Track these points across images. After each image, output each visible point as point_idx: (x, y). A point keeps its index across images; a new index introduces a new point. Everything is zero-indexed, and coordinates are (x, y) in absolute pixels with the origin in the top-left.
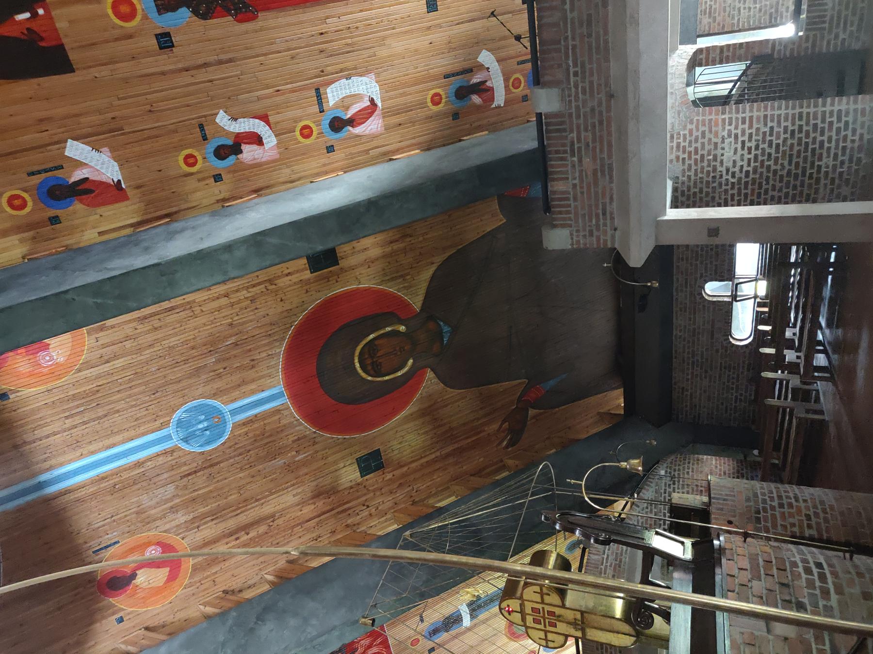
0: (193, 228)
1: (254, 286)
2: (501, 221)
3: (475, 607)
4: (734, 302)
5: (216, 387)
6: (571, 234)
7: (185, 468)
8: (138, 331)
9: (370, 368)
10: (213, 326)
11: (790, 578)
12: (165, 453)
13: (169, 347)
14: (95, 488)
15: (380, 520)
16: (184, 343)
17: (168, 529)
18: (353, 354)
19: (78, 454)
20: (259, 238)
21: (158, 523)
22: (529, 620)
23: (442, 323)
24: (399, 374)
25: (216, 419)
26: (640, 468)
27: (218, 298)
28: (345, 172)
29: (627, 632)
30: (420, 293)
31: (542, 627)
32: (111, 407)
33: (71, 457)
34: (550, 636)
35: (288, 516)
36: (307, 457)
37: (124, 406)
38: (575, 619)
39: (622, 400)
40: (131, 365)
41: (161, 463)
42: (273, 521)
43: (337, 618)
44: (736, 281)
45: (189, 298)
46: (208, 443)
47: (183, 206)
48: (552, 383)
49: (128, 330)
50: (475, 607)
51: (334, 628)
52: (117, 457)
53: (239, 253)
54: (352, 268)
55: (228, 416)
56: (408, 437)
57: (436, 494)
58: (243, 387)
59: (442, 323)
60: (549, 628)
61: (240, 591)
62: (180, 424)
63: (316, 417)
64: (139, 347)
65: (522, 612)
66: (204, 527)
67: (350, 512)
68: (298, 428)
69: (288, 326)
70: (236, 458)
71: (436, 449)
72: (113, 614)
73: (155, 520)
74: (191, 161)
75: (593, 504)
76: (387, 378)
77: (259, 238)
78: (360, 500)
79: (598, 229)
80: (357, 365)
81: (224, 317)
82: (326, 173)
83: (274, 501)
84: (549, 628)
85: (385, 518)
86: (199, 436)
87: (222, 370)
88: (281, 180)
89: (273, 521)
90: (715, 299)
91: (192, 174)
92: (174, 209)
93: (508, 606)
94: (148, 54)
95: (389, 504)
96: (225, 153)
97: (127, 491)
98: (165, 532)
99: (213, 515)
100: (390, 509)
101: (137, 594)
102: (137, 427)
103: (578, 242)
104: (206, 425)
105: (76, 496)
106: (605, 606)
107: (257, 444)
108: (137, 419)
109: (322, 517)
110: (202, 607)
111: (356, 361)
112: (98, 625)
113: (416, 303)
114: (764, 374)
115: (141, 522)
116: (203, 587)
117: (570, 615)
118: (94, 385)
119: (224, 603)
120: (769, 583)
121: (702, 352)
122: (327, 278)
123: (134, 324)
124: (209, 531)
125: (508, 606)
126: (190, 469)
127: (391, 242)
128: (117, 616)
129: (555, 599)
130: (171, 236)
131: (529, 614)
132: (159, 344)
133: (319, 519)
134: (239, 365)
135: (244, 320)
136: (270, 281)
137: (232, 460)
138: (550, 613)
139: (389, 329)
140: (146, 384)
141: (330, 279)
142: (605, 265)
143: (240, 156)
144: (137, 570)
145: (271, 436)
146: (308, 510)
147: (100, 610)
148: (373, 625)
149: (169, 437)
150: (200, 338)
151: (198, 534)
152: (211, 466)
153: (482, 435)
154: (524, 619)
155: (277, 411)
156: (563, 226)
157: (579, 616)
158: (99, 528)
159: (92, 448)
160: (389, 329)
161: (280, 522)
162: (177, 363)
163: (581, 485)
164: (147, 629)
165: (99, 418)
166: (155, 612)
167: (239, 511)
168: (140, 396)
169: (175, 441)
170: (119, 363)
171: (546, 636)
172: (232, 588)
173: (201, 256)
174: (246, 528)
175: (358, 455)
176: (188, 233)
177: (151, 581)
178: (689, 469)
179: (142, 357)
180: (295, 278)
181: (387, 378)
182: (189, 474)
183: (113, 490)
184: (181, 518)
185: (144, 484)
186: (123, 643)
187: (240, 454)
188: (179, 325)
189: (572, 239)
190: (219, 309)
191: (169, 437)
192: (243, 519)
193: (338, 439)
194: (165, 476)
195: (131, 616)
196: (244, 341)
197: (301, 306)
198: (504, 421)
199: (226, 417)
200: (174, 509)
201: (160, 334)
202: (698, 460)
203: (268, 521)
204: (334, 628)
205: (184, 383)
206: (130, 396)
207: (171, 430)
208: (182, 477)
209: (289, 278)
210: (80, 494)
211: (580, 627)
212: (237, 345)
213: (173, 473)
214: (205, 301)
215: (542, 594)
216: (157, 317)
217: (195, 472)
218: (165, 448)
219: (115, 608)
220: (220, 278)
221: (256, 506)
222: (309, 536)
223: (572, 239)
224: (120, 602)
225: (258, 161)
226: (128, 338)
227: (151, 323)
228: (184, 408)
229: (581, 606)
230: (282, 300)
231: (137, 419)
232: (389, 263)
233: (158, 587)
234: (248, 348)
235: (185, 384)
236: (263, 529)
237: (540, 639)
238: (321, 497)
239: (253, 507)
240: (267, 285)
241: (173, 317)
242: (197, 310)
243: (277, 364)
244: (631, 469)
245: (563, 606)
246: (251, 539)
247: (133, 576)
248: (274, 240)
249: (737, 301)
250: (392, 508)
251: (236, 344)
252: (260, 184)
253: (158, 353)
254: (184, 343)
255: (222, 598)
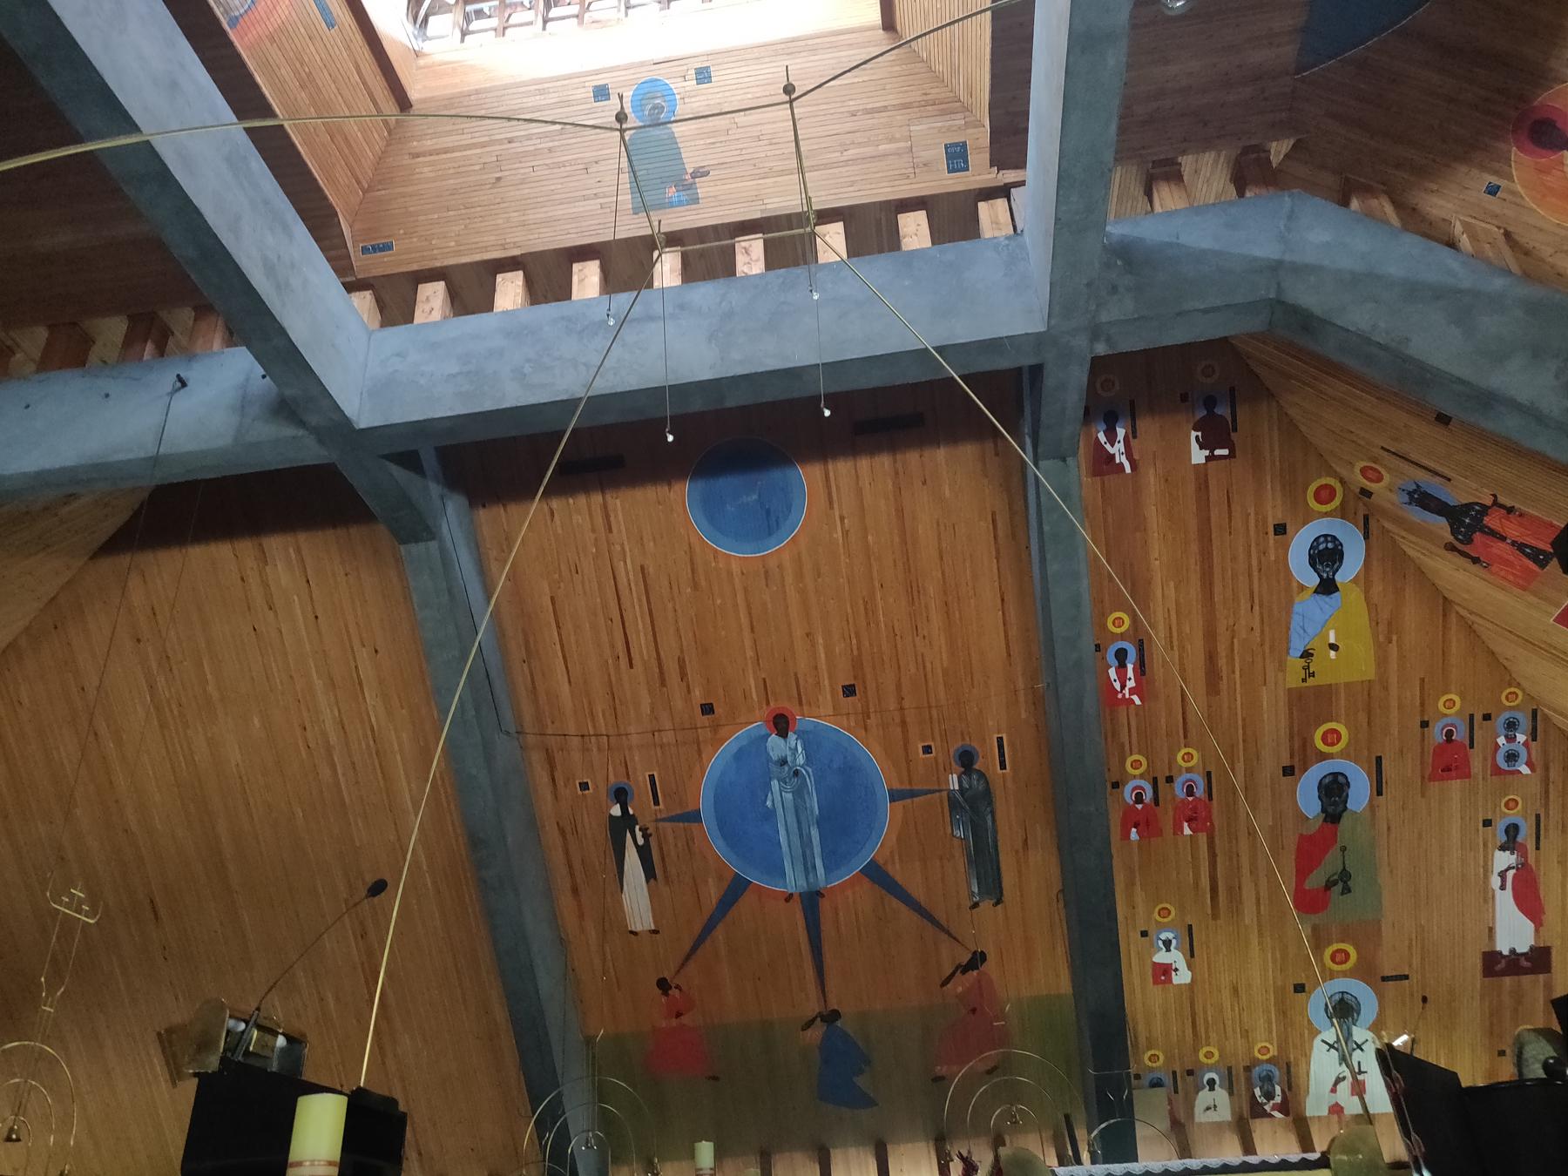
72: (1496, 173)
94: (780, 94)
128: (1495, 180)
164: (1507, 235)
195: (1509, 197)
219: (1506, 168)
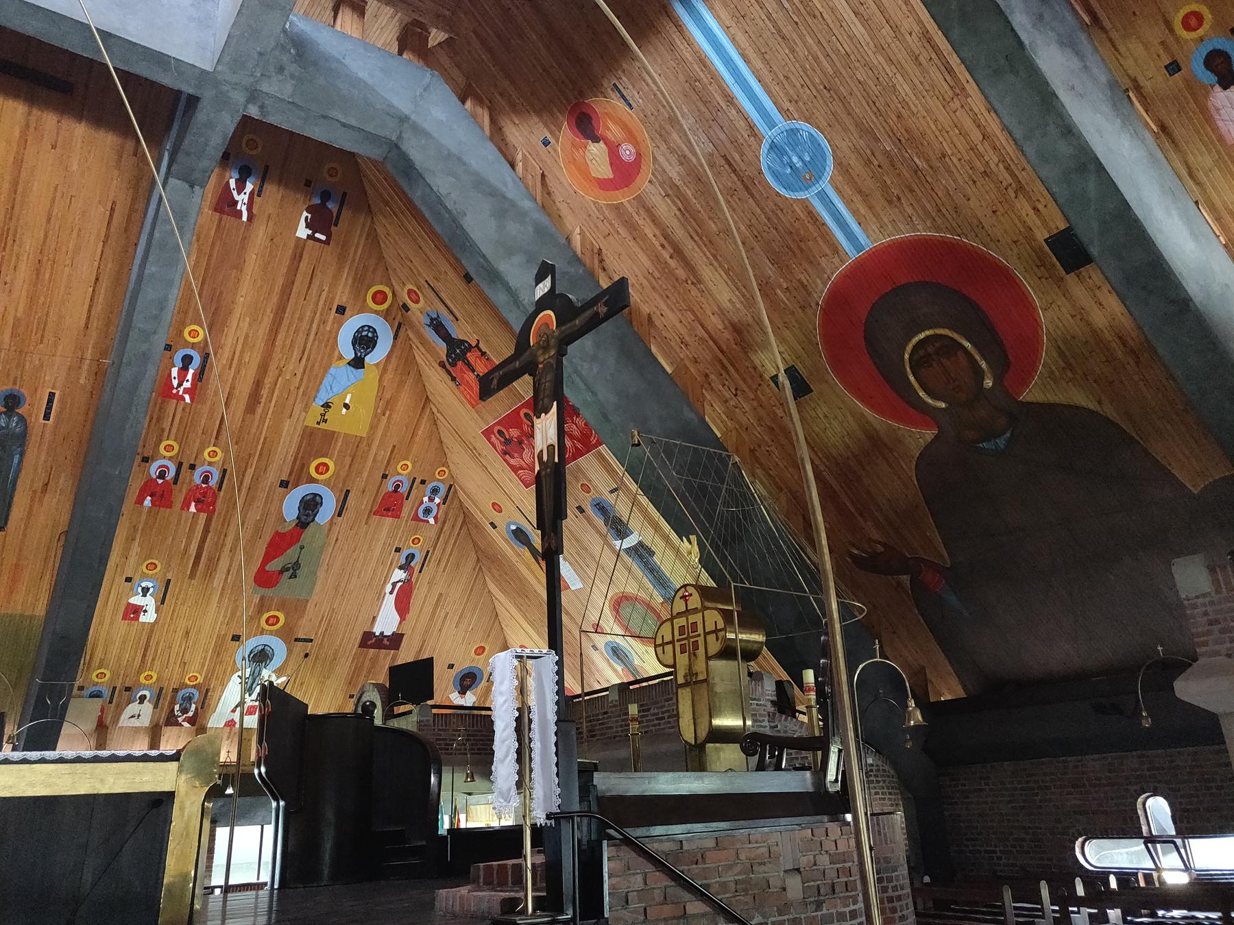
0: (1086, 67)
1: (1007, 168)
2: (1194, 486)
3: (641, 552)
4: (1143, 840)
5: (851, 162)
6: (1204, 595)
7: (737, 157)
8: (908, 37)
9: (921, 353)
10: (937, 133)
11: (841, 895)
12: (751, 127)
13: (894, 86)
14: (690, 59)
15: (722, 414)
16: (903, 104)
17: (657, 160)
18: (936, 327)
19: (728, 23)
20: (1092, 167)
21: (663, 147)
22: (681, 621)
23: (1008, 435)
24: (922, 394)
25: (811, 174)
26: (912, 722)
27: (979, 126)
28: (1225, 246)
29: (699, 735)
30: (1048, 396)
31: (677, 637)
32: (798, 41)
33: (723, 17)
34: (669, 648)
35: (702, 299)
36: (784, 302)
37: (801, 54)
38: (697, 674)
39: (949, 698)
40: (858, 46)
41: (738, 126)
42: (693, 283)
43: (607, 395)
44: (1179, 841)
45: (972, 88)
46: (775, 175)
47: (1114, 35)
48: (953, 599)
49: (907, 24)
50: (641, 552)
51: (594, 394)
52: (728, 62)
53: (1064, 148)
54: (1066, 294)
55: (815, 190)
56: (835, 424)
57: (770, 476)
58: (859, 198)
59: (1008, 435)
60: (677, 645)
61: (604, 269)
62: (793, 132)
63: (839, 299)
64: (886, 46)
65: (687, 612)
66: (669, 202)
67: (724, 374)
68: (819, 282)
69: (959, 230)
70: (763, 216)
71: (827, 463)
72: (551, 133)
73: (665, 141)
74: (1193, 22)
75: (858, 672)
76: (912, 378)
77: (1092, 167)
78: (741, 383)
79: (1222, 631)
80: (922, 336)
81: (952, 142)
82: (1218, 219)
83: (718, 276)
84: (677, 645)
85: (726, 419)
86: (782, 161)
87: (876, 163)
88: (1191, 158)
89: (693, 283)
90: (1140, 812)
91: (1171, 30)
92: (1107, 23)
93: (691, 595)
95: (744, 420)
96: (1217, 66)
97: (695, 97)
98: (654, 158)
99: (685, 209)
100: (739, 423)
101: (578, 149)
102: (774, 80)
103: (1195, 607)
104: (798, 165)
105: (677, 40)
106: (720, 706)
107: (787, 237)
108: (787, 78)
109: (711, 342)
110: (578, 230)
111: (928, 333)
112: (536, 119)
113: (1034, 393)
114: (1043, 884)
115: (661, 126)
116: (600, 224)
117: (700, 666)
118: (821, 10)
119: (588, 254)
120: (831, 874)
121: (1050, 800)
122: (1042, 263)
123: (916, 28)
124: (665, 210)
125: (691, 595)
126: (737, 165)
127: (1120, 338)
128: (550, 138)
129: (714, 646)
130: (1069, 43)
131: (687, 620)
132: (895, 71)
133: (708, 339)
134: (889, 182)
135: (955, 171)
136: (1020, 189)
137: (759, 211)
138: (696, 644)
139: (984, 365)
140: (837, 72)
141: (1042, 268)
142: (1160, 648)
143: (1218, 88)
144: (606, 143)
145: (802, 251)
146: (715, 322)
147: (552, 114)
148: (633, 445)
149: (771, 124)
150: (916, 121)
151: (659, 198)
152: (747, 188)
153: (860, 519)
154: (679, 615)
155: (836, 249)
156: (1216, 582)
157: (701, 677)
158: (644, 81)
159: (741, 38)
160: (984, 365)
161: (695, 292)
162: (874, 103)
163: (876, 657)
164: (543, 175)
165: (779, 31)
166: (562, 179)
167: (696, 238)
168: (819, 72)
169: (768, 134)
170: (858, 29)
171: (668, 643)
172: (605, 258)
173: (1047, 99)
174: (678, 252)
175: (799, 367)
176: (1075, 63)
177: (594, 161)
178: (882, 794)
179: (872, 57)
180: (1032, 219)
181: (912, 378)
182: (730, 164)
183: (692, 81)
184: (674, 172)
185: (708, 114)
186: (524, 155)
187: (769, 219)
188: (928, 88)
189: (1197, 597)
190: (963, 134)
191: (771, 124)
192: (689, 246)
193: (815, 337)
194: (722, 136)
195: (552, 152)
196: (924, 181)
197: (991, 240)
198: (884, 545)
199: (814, 188)
200: (683, 160)
201: (910, 68)
202: (897, 805)
203: (692, 277)
204: (594, 394)
205: (848, 121)
206: (816, 59)
207: (782, 124)
208: (725, 158)
209: (1031, 212)
210: (679, 43)
211: (689, 680)
212: (916, 172)
213: (728, 145)
214: (971, 110)
215: (716, 631)
216: (934, 56)
217: (734, 171)
218: (758, 125)
220: (1018, 134)
221: (708, 258)
222: (683, 331)
223: (1197, 597)
224: (567, 133)
225: (1217, 117)
226: (895, 28)
227: (922, 50)
228: (814, 131)
229: (713, 678)
230: (994, 212)
231: (787, 78)
232: (1086, 342)
233: (590, 173)
234: (916, 188)
235: (847, 122)
236: (681, 273)
237: (663, 636)
238: (735, 334)
239: (705, 255)
240: (1014, 185)
241: (936, 75)
242: (956, 104)
243: (899, 231)
244: (909, 713)
245: (708, 658)
246: (666, 262)
247: (596, 139)
248: (1092, 186)
249: (1146, 843)
250: (741, 426)
251: (916, 170)
252: (1177, 131)
253: (883, 74)
254: (903, 104)
255: (592, 250)
